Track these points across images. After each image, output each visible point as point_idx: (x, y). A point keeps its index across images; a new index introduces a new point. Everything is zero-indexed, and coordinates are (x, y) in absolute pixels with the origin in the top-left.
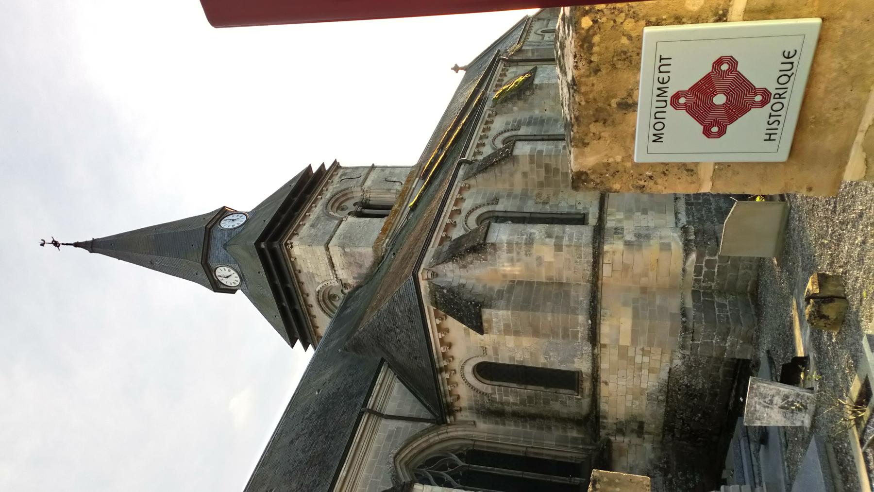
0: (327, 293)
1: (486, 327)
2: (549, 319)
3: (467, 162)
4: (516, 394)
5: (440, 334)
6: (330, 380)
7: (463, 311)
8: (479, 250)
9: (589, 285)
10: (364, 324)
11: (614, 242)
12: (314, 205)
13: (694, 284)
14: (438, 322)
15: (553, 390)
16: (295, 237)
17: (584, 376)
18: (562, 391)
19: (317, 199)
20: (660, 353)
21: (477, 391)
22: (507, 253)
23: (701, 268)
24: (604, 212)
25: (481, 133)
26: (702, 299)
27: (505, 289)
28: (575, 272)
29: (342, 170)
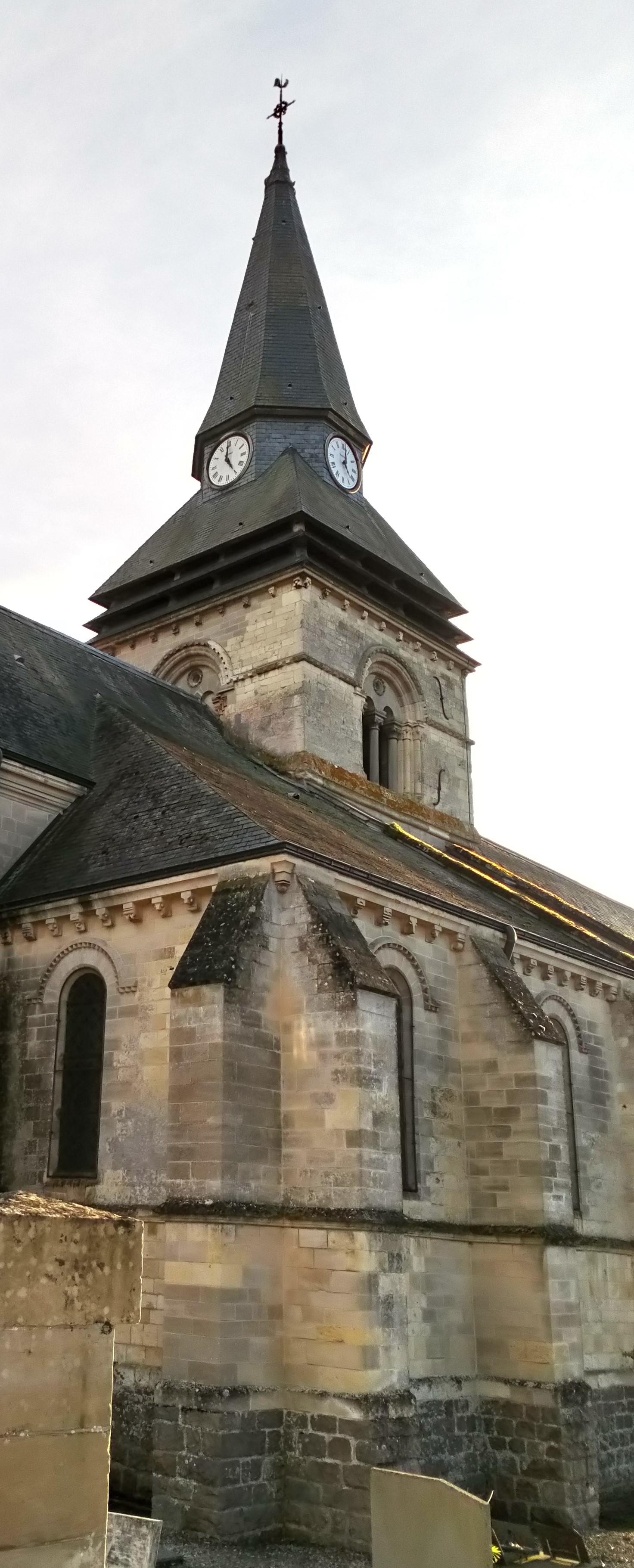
0: (205, 663)
1: (184, 994)
2: (211, 1120)
3: (509, 945)
4: (45, 1053)
5: (160, 900)
6: (42, 680)
7: (215, 946)
8: (340, 975)
9: (279, 1200)
10: (160, 746)
11: (373, 1254)
12: (384, 625)
13: (295, 1415)
14: (186, 896)
15: (56, 1126)
16: (318, 593)
17: (88, 1189)
18: (55, 1145)
19: (397, 630)
20: (147, 1343)
21: (46, 976)
22: (338, 1034)
23: (331, 1430)
24: (422, 1231)
25: (569, 971)
26: (267, 1430)
27: (263, 1031)
28: (306, 1172)
29: (458, 678)
